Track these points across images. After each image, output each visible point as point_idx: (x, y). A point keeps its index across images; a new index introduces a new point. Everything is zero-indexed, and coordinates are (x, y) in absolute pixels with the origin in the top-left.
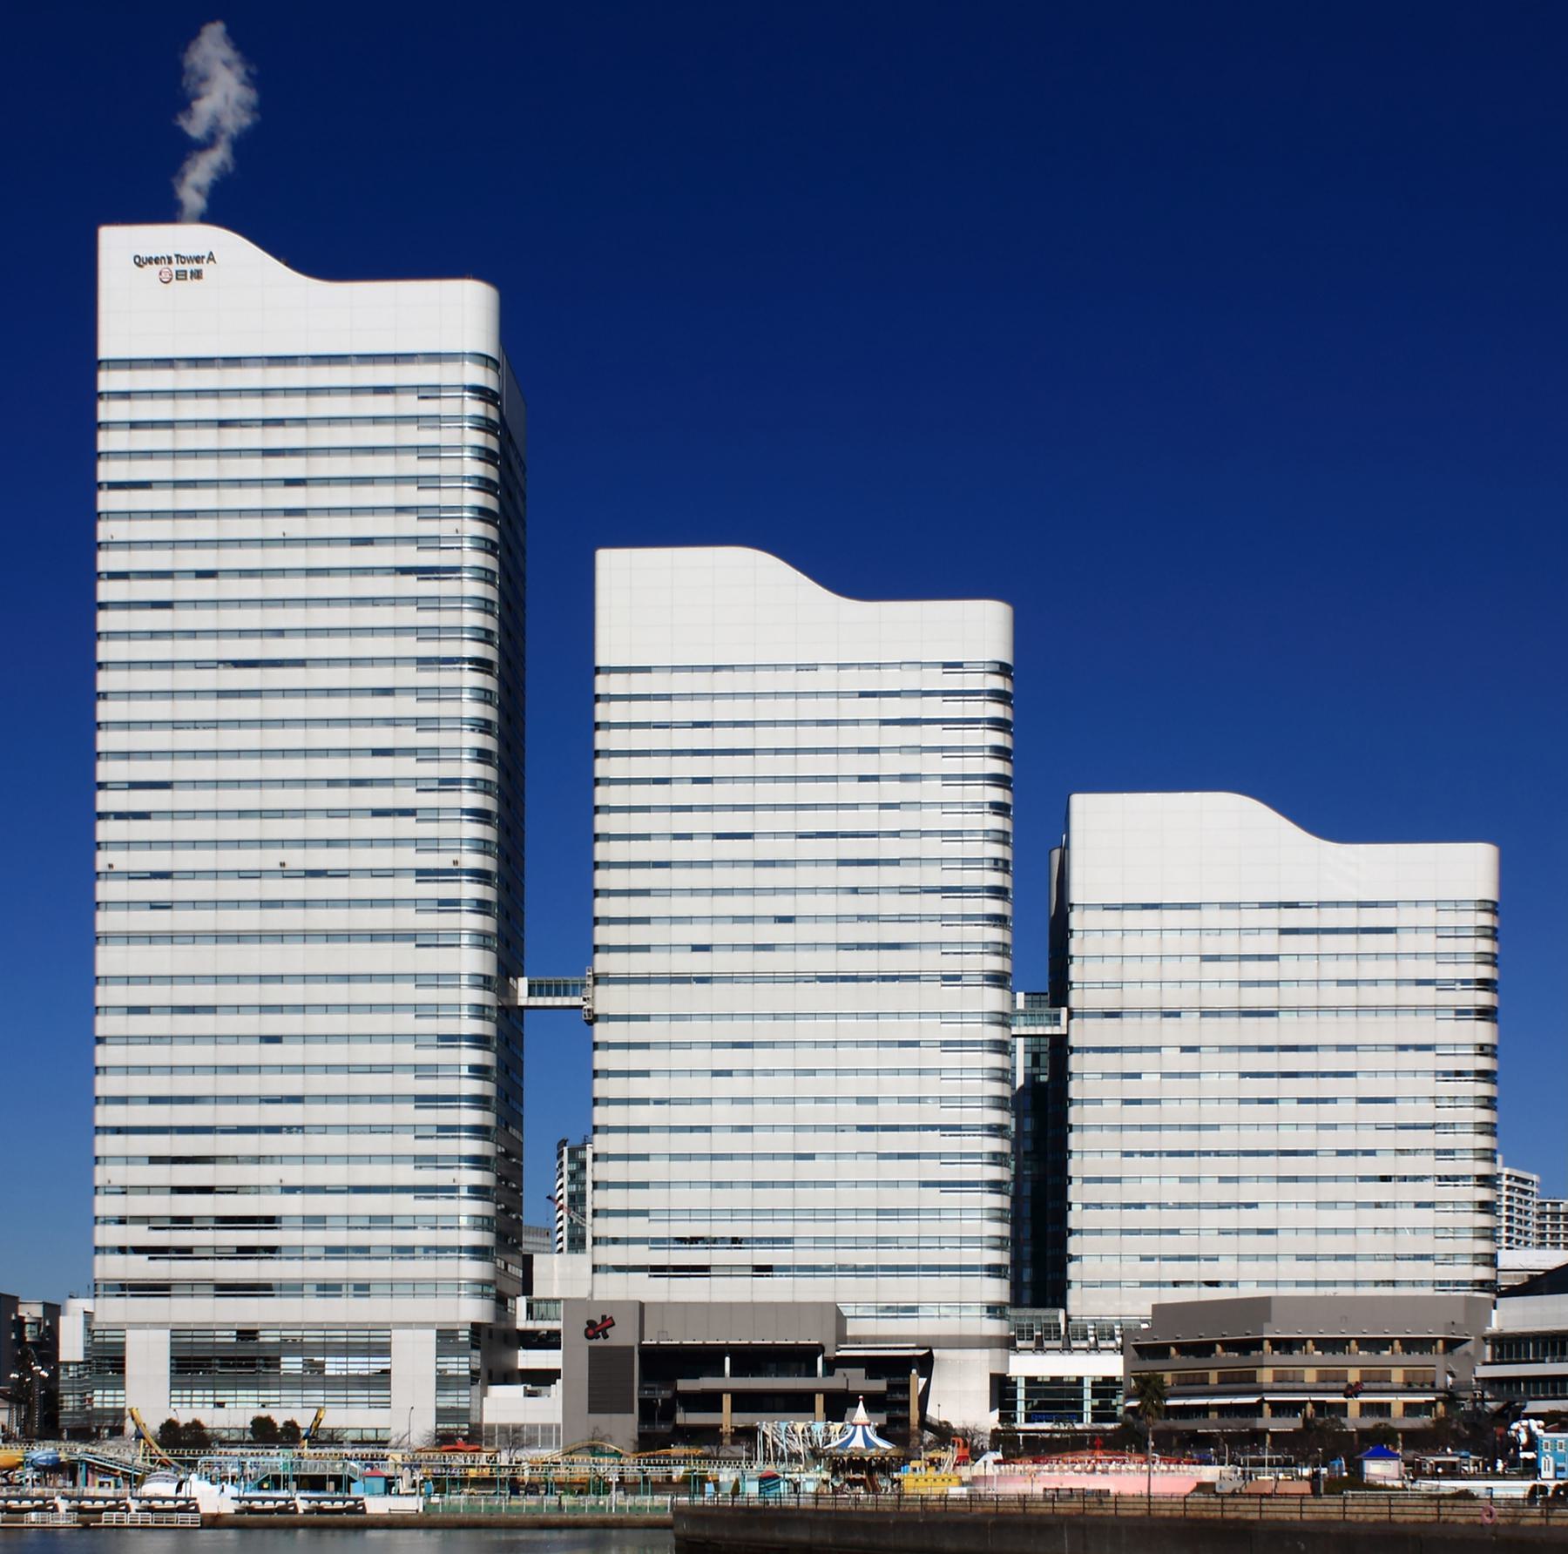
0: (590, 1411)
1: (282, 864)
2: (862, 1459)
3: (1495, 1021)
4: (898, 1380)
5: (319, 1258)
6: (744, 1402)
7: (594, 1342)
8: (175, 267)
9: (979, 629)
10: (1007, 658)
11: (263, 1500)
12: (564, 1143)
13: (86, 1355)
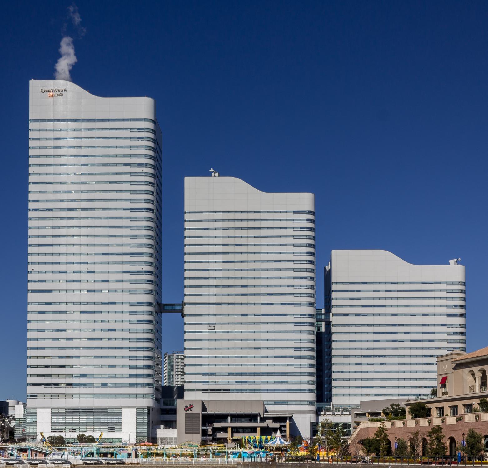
0: (186, 433)
1: (88, 269)
2: (280, 448)
3: (465, 317)
4: (283, 424)
5: (99, 387)
6: (235, 430)
7: (187, 412)
8: (54, 93)
9: (305, 200)
10: (312, 209)
11: (90, 460)
12: (167, 353)
13: (23, 417)
